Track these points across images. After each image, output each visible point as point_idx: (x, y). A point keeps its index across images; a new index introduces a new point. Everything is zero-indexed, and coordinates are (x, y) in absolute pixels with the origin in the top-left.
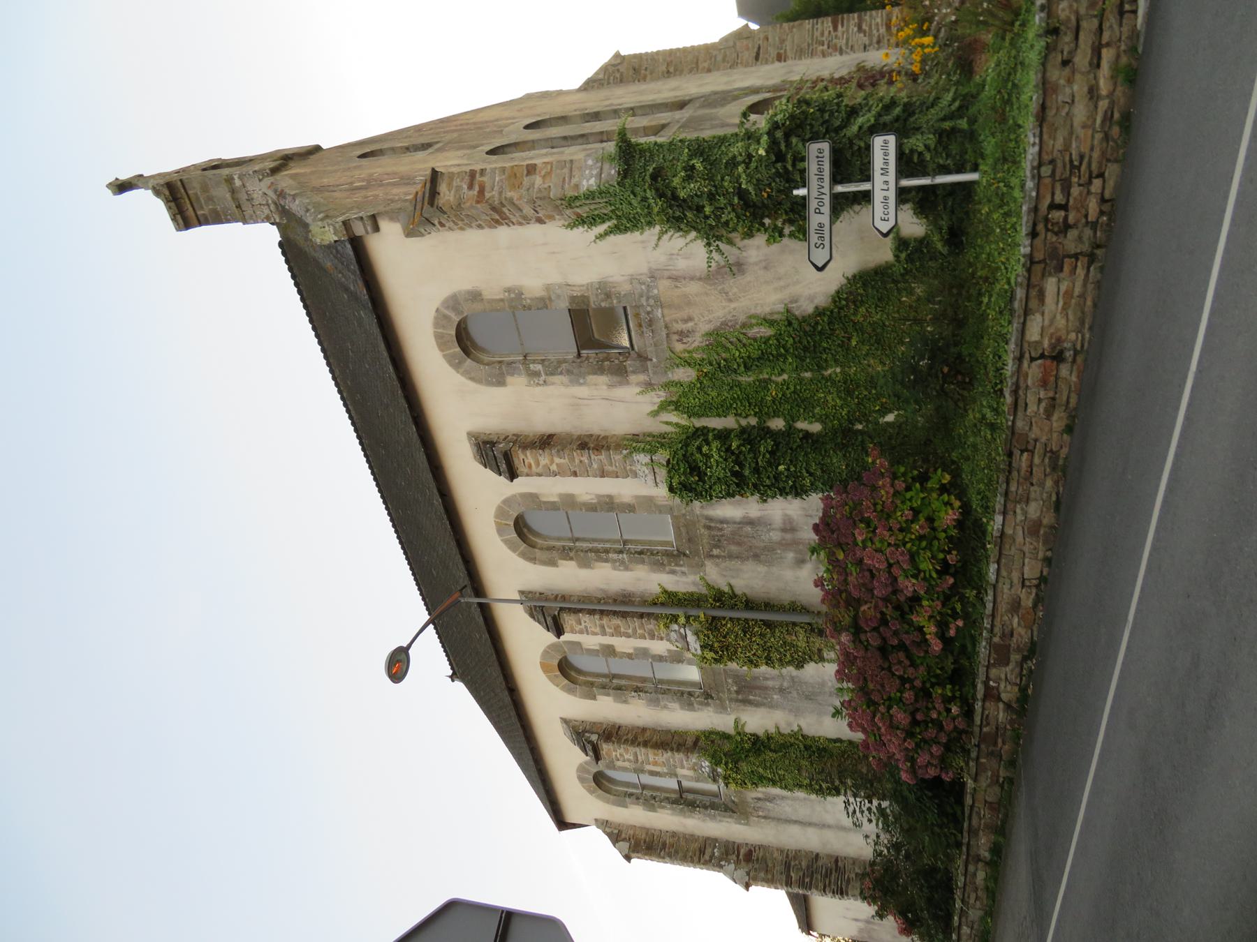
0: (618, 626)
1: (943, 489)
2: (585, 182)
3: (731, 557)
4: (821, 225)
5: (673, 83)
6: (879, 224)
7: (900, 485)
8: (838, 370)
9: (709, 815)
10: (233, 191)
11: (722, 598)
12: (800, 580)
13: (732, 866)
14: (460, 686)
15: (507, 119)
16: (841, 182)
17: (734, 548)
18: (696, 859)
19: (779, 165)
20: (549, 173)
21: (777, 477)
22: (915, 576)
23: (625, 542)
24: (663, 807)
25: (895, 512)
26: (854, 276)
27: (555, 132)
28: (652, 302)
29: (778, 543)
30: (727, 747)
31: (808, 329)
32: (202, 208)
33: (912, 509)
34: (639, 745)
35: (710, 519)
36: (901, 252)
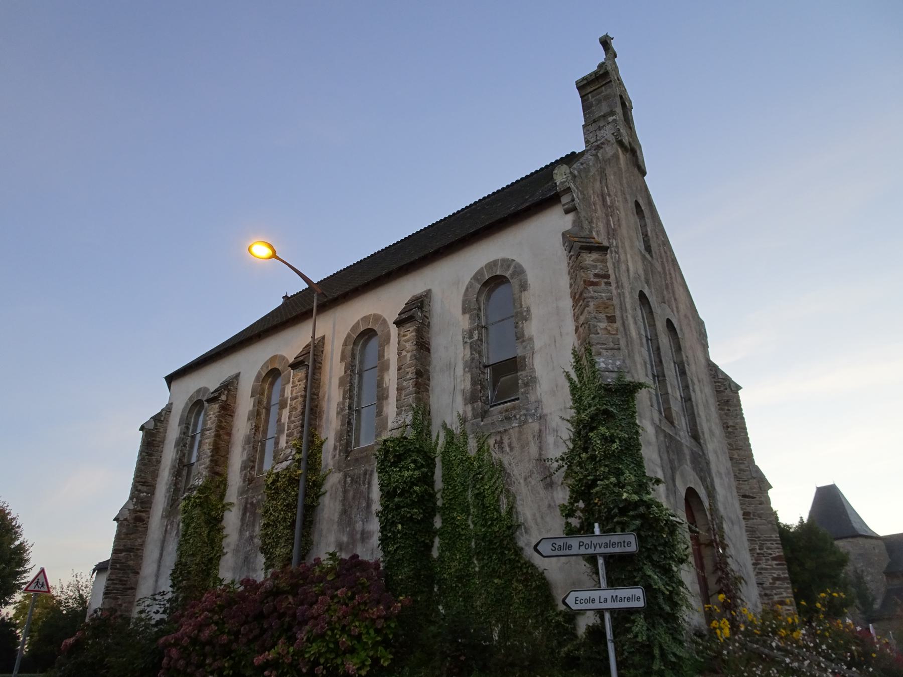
0: (296, 409)
1: (376, 661)
2: (602, 359)
3: (345, 492)
4: (570, 547)
5: (718, 431)
6: (573, 595)
7: (380, 624)
8: (477, 569)
9: (170, 488)
10: (604, 116)
11: (314, 489)
12: (327, 544)
13: (132, 507)
14: (280, 302)
15: (677, 308)
16: (607, 563)
17: (351, 494)
18: (138, 480)
19: (616, 510)
20: (609, 333)
21: (394, 524)
22: (308, 640)
23: (358, 412)
24: (177, 453)
25: (358, 621)
26: (544, 579)
27: (664, 340)
28: (523, 418)
29: (350, 529)
30: (213, 498)
31: (505, 542)
32: (593, 97)
33: (360, 635)
34: (217, 431)
35: (371, 475)
36: (563, 617)
